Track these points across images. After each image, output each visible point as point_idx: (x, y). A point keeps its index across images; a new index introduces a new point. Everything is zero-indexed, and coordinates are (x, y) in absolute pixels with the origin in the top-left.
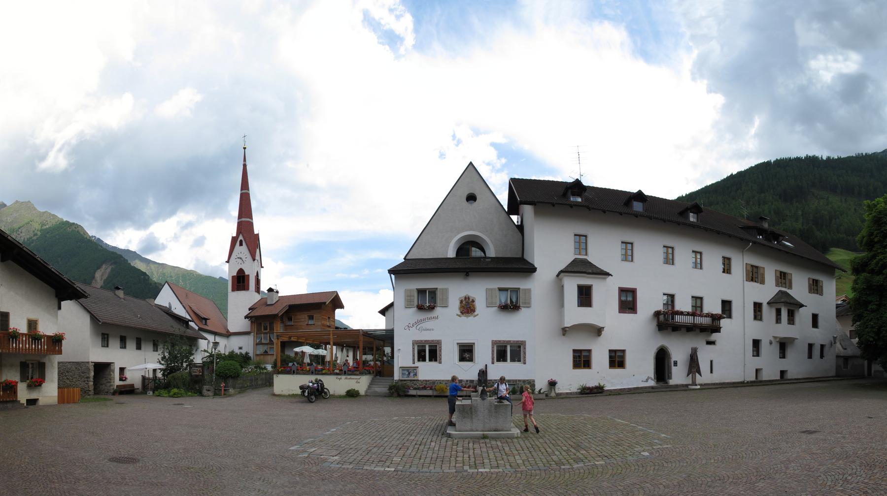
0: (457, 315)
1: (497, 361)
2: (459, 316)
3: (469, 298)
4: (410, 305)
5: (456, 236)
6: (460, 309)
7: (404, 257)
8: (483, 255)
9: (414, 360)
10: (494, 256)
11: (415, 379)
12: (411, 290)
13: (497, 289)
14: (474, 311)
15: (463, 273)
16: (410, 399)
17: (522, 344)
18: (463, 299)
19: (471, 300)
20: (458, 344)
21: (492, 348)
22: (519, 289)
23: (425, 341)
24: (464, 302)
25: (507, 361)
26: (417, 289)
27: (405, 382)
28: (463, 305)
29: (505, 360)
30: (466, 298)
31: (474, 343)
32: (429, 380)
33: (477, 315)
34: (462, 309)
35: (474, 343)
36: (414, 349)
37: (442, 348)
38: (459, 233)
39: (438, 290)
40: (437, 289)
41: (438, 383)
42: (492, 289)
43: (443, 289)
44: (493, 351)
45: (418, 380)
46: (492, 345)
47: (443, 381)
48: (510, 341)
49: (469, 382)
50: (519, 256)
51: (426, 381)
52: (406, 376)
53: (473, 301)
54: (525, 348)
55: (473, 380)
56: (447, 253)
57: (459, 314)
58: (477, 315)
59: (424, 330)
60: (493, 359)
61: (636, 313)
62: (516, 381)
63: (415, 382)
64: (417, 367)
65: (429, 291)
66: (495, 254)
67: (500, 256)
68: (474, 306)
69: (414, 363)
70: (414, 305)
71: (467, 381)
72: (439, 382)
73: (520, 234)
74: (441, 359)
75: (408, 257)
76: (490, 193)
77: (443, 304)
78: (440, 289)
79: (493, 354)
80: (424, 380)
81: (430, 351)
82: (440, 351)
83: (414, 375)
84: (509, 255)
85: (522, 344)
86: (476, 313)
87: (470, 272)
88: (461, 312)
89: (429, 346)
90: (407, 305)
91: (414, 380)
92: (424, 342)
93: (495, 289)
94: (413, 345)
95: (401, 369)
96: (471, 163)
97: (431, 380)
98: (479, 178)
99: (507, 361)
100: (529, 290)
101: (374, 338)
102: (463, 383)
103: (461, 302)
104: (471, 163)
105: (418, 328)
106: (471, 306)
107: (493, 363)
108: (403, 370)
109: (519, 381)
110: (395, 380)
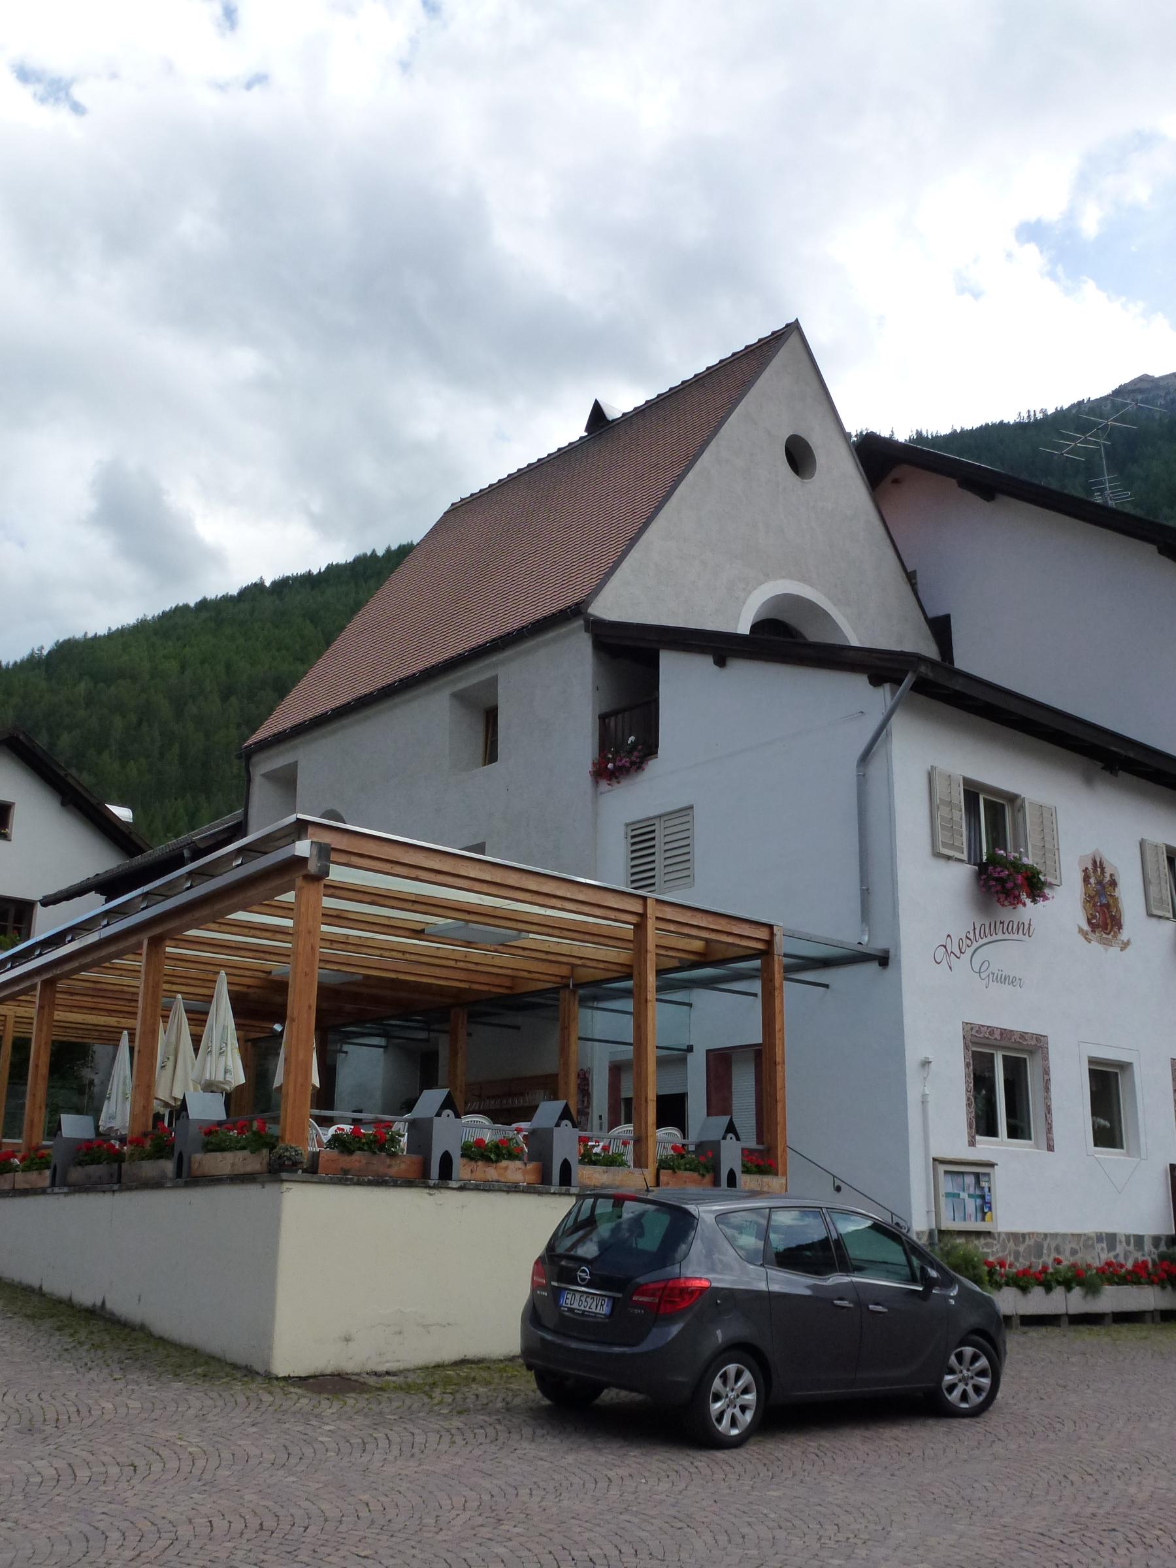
18: (1090, 867)
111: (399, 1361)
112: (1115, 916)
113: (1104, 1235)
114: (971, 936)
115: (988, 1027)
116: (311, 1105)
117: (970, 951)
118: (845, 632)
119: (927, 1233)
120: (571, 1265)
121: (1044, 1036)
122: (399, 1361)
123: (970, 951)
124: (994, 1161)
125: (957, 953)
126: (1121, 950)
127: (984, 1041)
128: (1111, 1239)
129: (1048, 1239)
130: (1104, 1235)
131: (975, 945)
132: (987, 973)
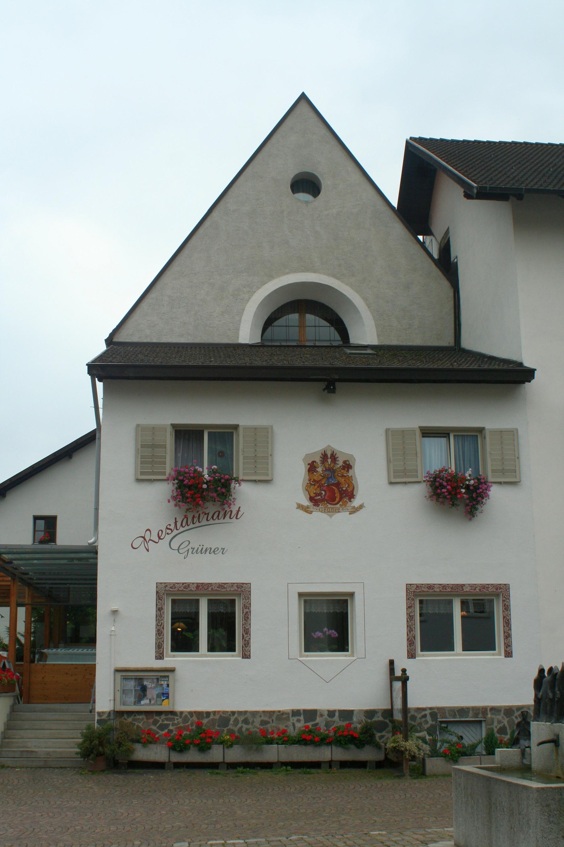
0: (300, 507)
1: (422, 650)
2: (306, 509)
3: (334, 457)
4: (153, 473)
5: (264, 283)
6: (307, 489)
7: (107, 336)
8: (338, 337)
9: (159, 646)
10: (377, 344)
11: (165, 706)
12: (153, 429)
13: (418, 433)
14: (351, 496)
15: (315, 384)
16: (151, 776)
17: (239, 595)
18: (318, 460)
19: (340, 463)
20: (301, 595)
21: (409, 607)
22: (481, 430)
23: (199, 586)
24: (320, 470)
25: (197, 650)
26: (173, 426)
27: (130, 719)
28: (316, 477)
29: (448, 646)
30: (324, 456)
31: (352, 595)
32: (208, 714)
33: (361, 507)
34: (314, 490)
35: (352, 595)
36: (159, 609)
37: (253, 608)
38: (271, 277)
39: (241, 430)
40: (236, 427)
41: (236, 721)
42: (403, 433)
43: (501, 432)
44: (410, 618)
45: (173, 713)
46: (408, 599)
47: (254, 714)
48: (463, 586)
49: (336, 718)
50: (447, 341)
51: (199, 714)
52: (132, 699)
53: (348, 466)
54: (507, 608)
55: (351, 712)
56: (238, 329)
57: (306, 502)
58: (361, 507)
59: (195, 551)
60: (411, 642)
61: (33, 516)
62: (484, 710)
63: (161, 720)
64: (172, 670)
65: (210, 434)
66: (379, 336)
67: (394, 342)
68: (350, 481)
69: (160, 656)
70: (164, 473)
71: (331, 713)
72: (241, 718)
73: (445, 284)
74: (247, 644)
75: (122, 337)
76: (357, 176)
77: (256, 473)
78: (246, 428)
79: (247, 631)
80: (191, 713)
81: (213, 619)
82: (247, 617)
83: (158, 696)
84: (417, 341)
85: (498, 595)
86: (356, 503)
87: (340, 380)
88: (311, 499)
89: (210, 602)
90: (142, 473)
91: (159, 713)
92: (193, 588)
93: (412, 431)
94: (159, 597)
95: (119, 675)
96: (303, 97)
97: (214, 712)
98: (329, 134)
99: (197, 650)
100: (513, 434)
101: (13, 576)
102: (318, 720)
103: (312, 468)
104: (303, 97)
105: (175, 544)
106: (342, 480)
107: (411, 655)
108: (125, 678)
109: (494, 710)
110: (99, 714)
111: (180, 772)
112: (346, 490)
113: (302, 712)
114: (172, 527)
115: (183, 584)
116: (171, 650)
117: (168, 538)
118: (373, 323)
119: (108, 713)
120: (445, 725)
121: (246, 584)
122: (180, 772)
123: (168, 538)
124: (387, 662)
125: (156, 539)
126: (350, 514)
127: (235, 592)
128: (311, 714)
129: (236, 715)
130: (302, 712)
131: (176, 532)
132: (186, 549)
